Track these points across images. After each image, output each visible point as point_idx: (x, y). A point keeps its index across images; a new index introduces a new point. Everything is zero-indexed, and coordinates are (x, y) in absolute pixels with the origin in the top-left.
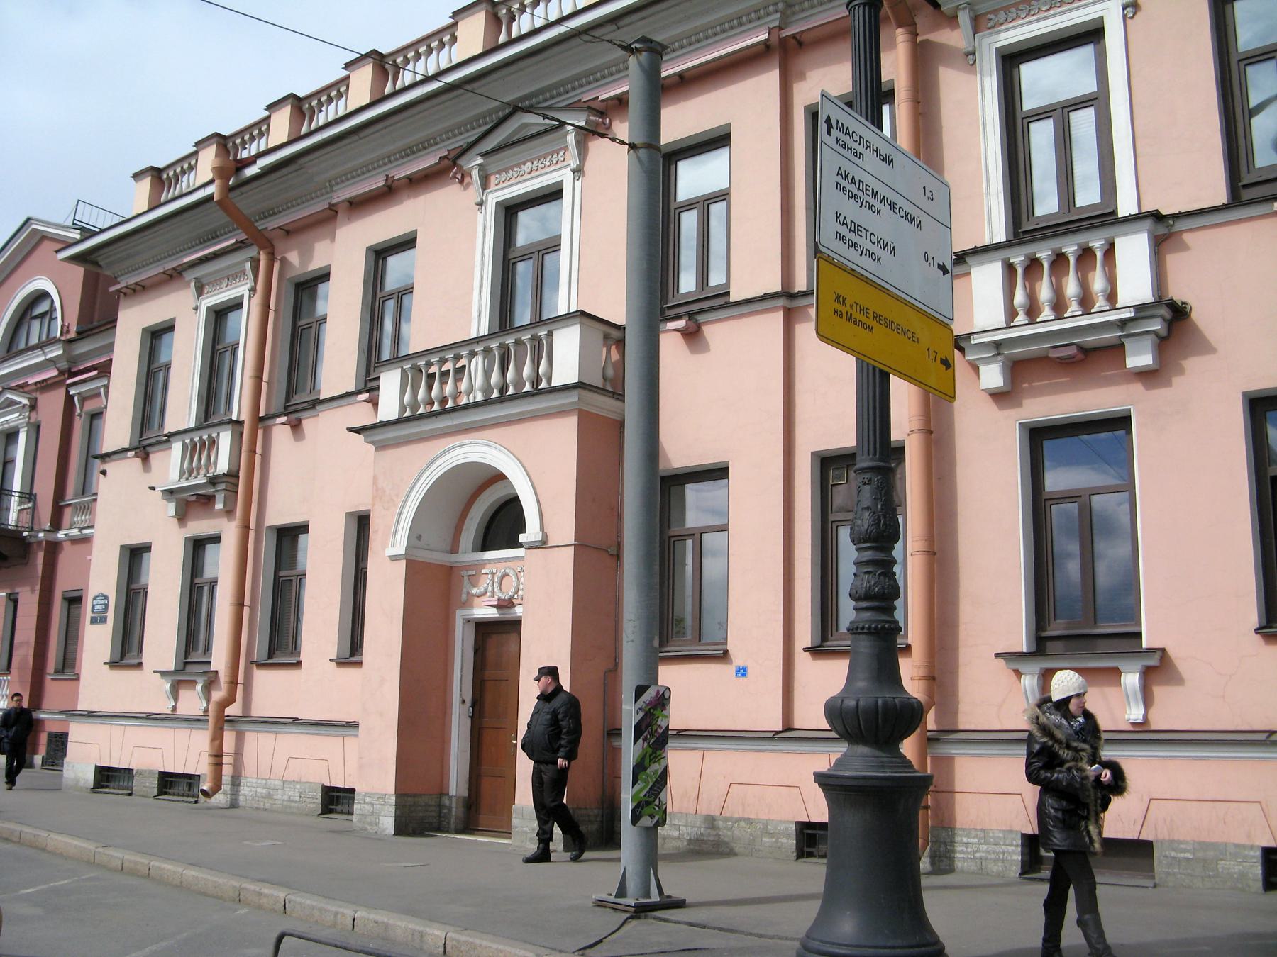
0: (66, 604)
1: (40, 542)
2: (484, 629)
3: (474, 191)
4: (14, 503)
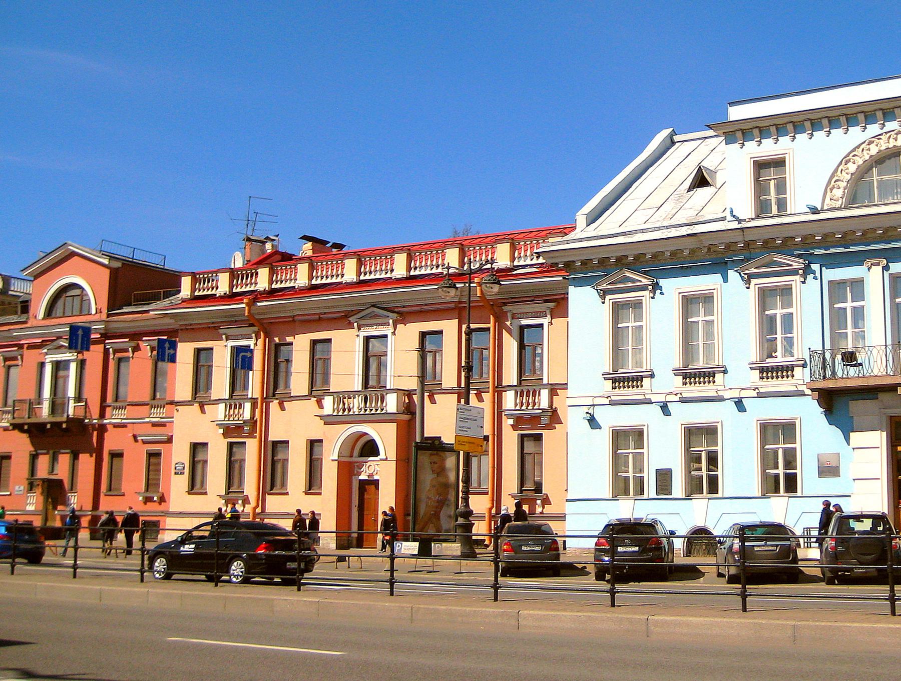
0: (110, 456)
1: (94, 425)
2: (362, 482)
3: (354, 331)
4: (72, 404)
